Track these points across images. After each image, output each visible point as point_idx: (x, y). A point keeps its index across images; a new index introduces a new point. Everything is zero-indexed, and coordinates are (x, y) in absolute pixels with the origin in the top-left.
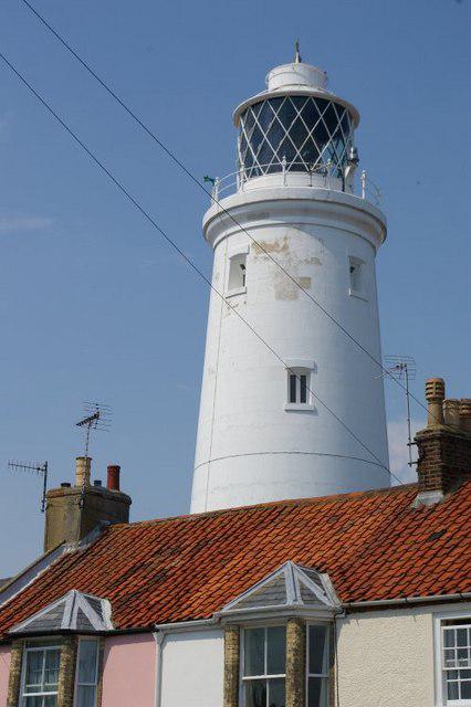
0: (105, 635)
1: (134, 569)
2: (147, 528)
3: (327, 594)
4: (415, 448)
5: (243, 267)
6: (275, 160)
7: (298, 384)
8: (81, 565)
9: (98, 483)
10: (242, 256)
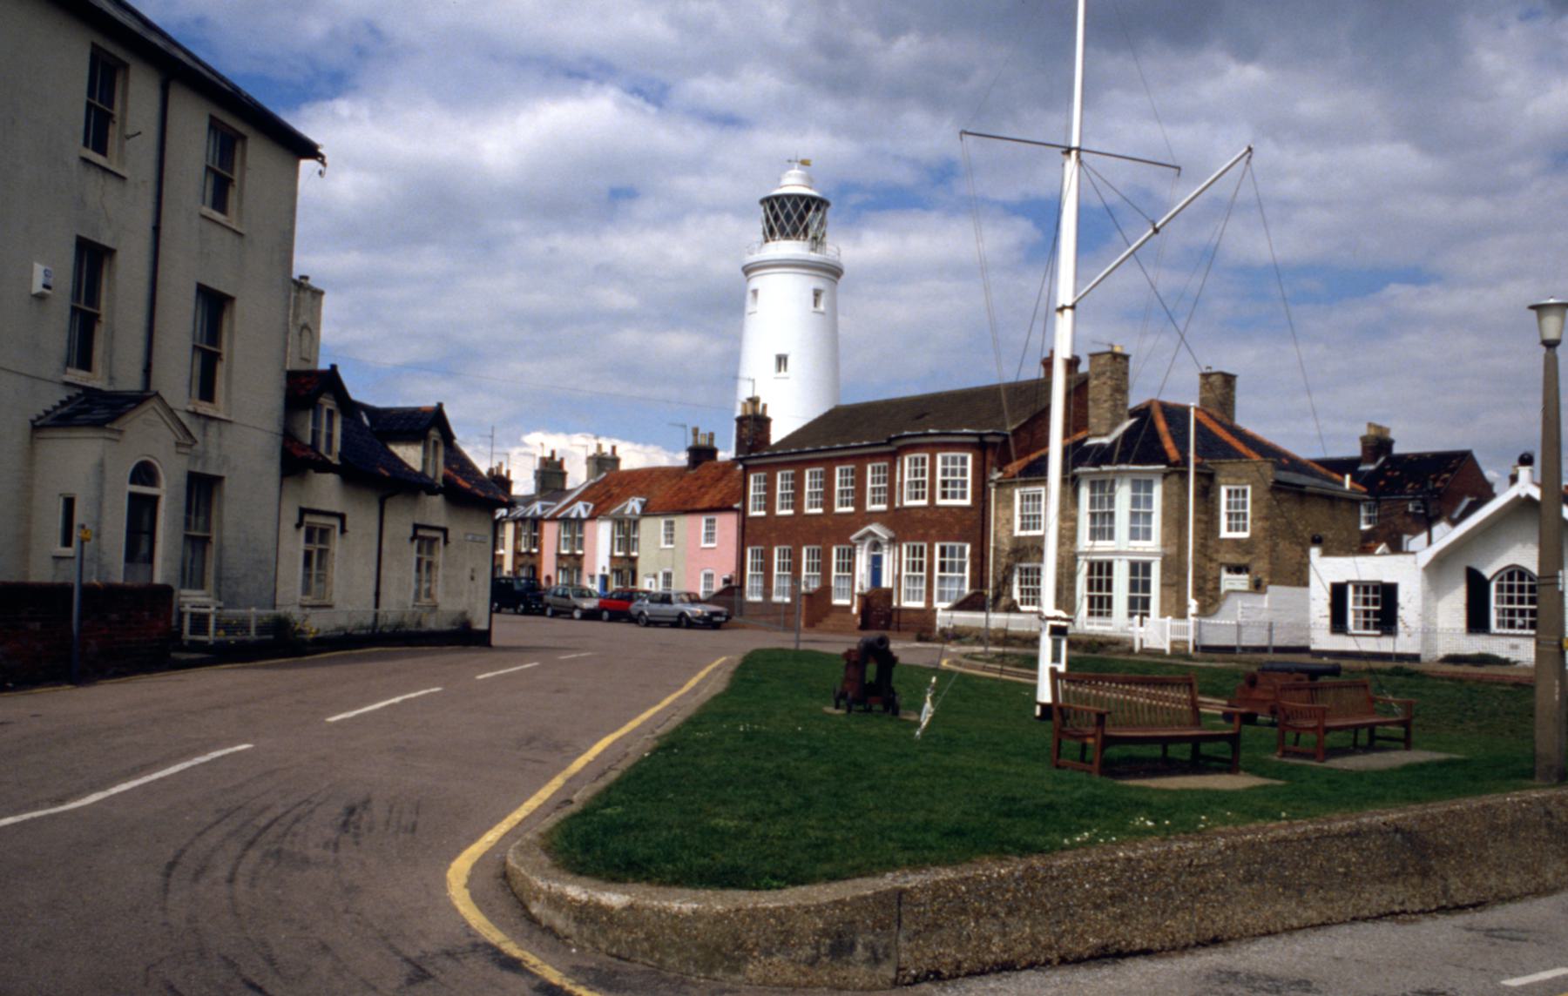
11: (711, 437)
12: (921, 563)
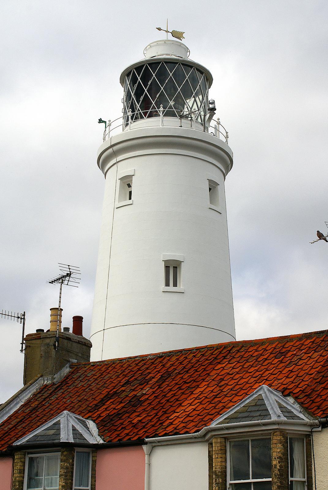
0: (97, 448)
1: (108, 397)
2: (95, 364)
3: (93, 434)
5: (129, 186)
6: (154, 108)
7: (172, 270)
8: (60, 393)
9: (67, 329)
10: (130, 177)
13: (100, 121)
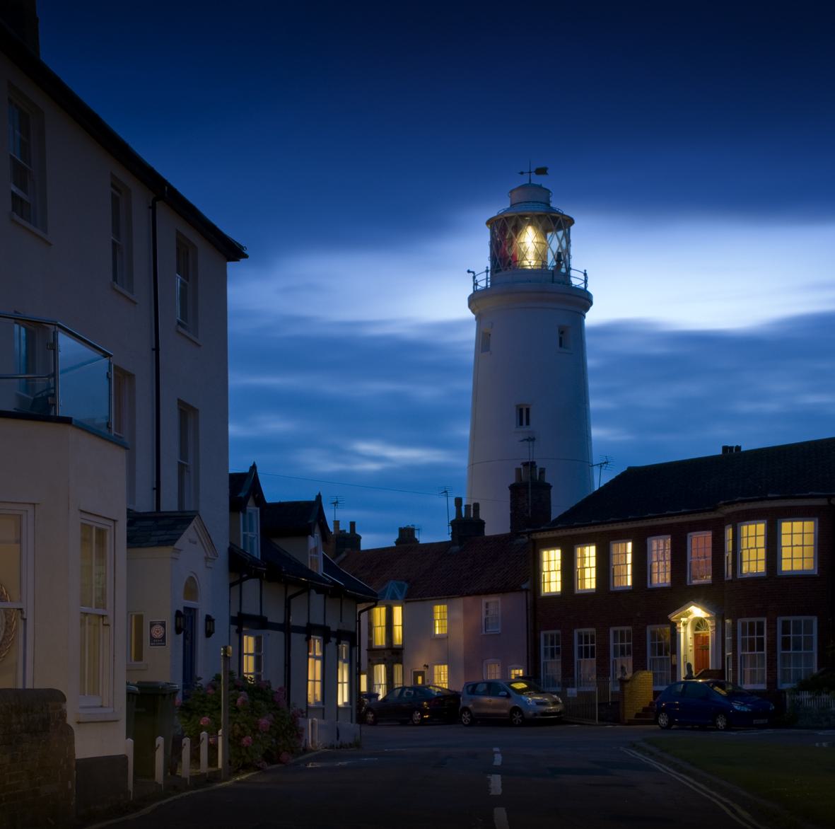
4: (450, 527)
11: (476, 506)
12: (761, 641)
13: (469, 272)
